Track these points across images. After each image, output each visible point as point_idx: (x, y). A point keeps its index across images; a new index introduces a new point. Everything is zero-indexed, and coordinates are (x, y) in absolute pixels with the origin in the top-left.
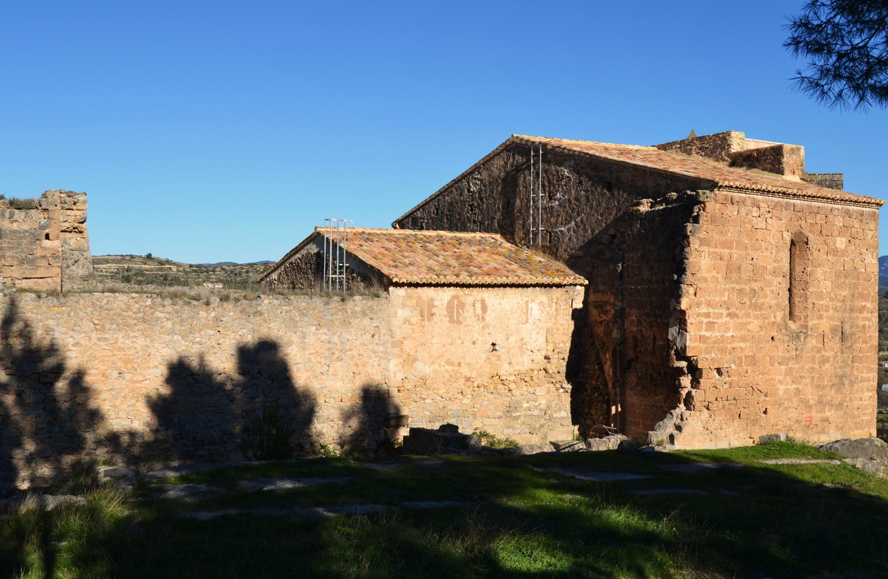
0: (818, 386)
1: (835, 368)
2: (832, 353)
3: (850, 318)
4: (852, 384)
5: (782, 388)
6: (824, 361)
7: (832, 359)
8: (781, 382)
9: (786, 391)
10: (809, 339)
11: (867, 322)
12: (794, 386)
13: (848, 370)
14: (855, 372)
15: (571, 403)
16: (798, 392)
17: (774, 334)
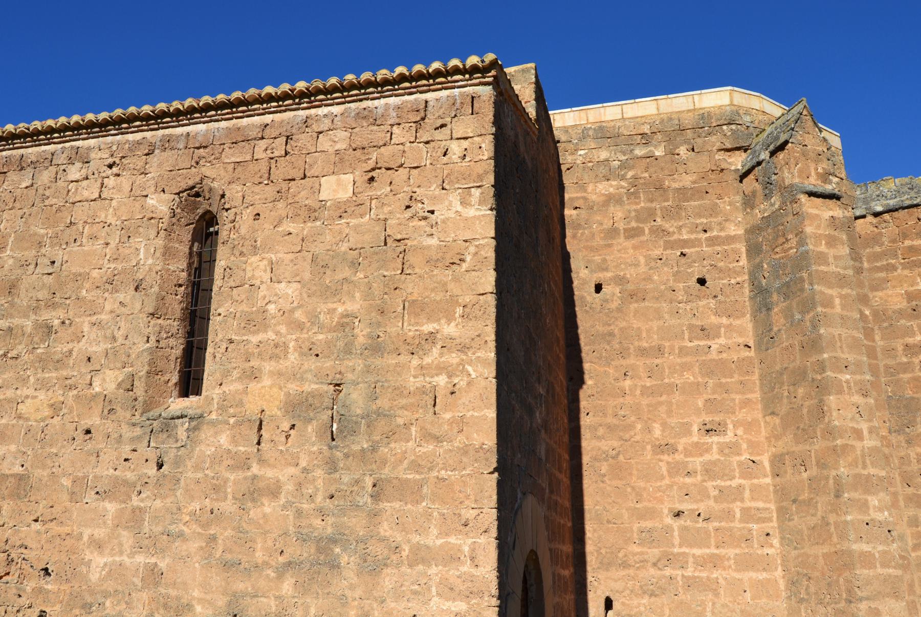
0: (227, 566)
1: (299, 513)
2: (292, 470)
3: (368, 370)
4: (372, 568)
5: (99, 562)
6: (254, 492)
7: (290, 487)
8: (98, 545)
9: (115, 572)
10: (206, 433)
11: (441, 380)
12: (140, 559)
13: (356, 523)
14: (385, 529)
15: (496, 347)
16: (154, 575)
17: (93, 420)
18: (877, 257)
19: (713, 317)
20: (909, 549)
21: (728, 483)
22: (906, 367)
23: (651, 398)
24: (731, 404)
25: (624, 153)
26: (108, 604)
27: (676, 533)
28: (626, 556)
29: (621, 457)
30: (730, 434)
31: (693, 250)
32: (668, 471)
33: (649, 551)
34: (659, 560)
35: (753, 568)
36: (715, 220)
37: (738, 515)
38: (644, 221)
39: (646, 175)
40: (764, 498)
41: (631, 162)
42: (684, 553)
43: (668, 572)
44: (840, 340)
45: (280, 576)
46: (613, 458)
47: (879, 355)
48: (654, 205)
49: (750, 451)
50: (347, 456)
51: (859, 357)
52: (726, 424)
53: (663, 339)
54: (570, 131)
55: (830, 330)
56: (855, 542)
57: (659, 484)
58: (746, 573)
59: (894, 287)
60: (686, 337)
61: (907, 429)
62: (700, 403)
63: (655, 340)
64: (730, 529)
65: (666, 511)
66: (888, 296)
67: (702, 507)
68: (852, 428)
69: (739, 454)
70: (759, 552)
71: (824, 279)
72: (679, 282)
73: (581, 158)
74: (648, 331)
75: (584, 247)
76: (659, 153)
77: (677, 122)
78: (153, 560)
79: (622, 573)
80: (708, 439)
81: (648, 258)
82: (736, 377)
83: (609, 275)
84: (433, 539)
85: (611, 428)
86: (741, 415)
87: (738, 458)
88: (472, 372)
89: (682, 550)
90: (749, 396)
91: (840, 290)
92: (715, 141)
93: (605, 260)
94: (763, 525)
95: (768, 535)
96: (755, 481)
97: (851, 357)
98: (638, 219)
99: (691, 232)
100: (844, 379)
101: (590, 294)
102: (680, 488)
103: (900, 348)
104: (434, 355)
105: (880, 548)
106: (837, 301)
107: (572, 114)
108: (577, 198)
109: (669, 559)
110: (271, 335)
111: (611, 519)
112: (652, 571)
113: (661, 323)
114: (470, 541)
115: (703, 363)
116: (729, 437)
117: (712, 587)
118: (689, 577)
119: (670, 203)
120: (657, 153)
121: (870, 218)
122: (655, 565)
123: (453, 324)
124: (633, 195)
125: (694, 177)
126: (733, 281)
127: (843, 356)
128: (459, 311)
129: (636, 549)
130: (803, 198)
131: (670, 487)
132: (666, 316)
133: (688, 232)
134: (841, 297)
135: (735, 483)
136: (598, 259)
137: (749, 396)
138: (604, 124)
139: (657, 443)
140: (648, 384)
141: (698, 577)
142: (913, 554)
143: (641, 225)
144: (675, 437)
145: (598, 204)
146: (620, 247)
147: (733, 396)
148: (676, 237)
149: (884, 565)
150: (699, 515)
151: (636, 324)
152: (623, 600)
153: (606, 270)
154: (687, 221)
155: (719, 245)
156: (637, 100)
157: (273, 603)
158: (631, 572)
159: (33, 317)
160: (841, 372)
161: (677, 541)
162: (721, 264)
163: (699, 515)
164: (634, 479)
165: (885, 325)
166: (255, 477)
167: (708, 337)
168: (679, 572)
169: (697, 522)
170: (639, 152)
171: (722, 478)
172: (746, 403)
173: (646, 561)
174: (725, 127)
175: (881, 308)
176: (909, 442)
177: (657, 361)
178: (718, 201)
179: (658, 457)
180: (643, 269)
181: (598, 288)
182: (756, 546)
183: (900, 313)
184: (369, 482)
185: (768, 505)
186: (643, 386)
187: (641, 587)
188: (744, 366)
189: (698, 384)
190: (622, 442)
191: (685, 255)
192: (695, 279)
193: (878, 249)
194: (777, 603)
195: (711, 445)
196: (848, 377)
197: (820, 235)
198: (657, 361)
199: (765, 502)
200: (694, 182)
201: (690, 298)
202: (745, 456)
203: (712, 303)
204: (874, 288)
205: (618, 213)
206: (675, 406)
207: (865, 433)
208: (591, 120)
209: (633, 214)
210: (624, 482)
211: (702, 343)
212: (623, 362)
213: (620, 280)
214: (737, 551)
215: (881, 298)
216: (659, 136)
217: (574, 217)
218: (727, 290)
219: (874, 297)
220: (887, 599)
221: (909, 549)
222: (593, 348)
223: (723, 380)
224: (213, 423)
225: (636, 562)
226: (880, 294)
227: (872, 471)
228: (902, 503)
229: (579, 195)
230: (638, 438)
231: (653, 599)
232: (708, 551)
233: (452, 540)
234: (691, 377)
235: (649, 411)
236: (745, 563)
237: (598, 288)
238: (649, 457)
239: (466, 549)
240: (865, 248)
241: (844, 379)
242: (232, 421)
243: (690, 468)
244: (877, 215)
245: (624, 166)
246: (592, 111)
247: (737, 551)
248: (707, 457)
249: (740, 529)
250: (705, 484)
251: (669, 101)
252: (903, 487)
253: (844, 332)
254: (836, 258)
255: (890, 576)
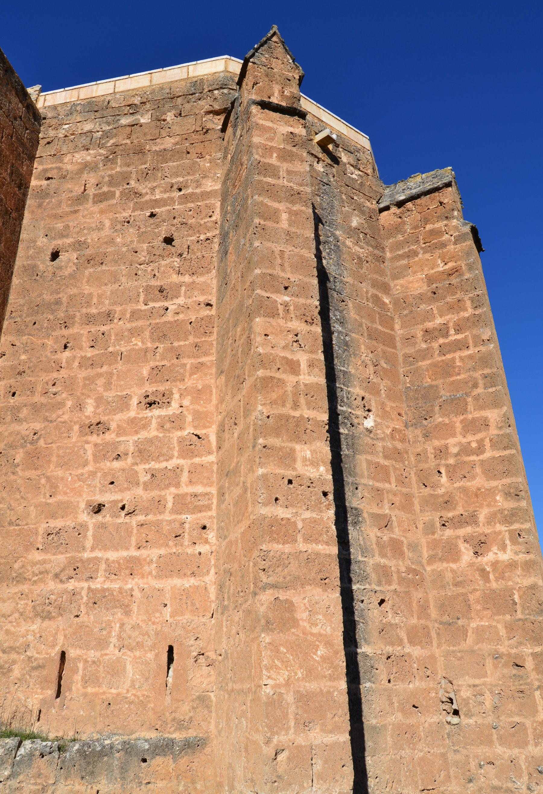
18: (399, 245)
19: (175, 276)
20: (424, 562)
21: (164, 465)
22: (425, 354)
23: (89, 370)
24: (182, 371)
25: (109, 124)
27: (90, 533)
28: (23, 566)
29: (41, 442)
30: (175, 405)
31: (164, 209)
32: (94, 456)
33: (53, 558)
34: (63, 570)
35: (180, 573)
36: (192, 178)
37: (170, 505)
38: (117, 185)
39: (128, 141)
40: (205, 481)
41: (114, 131)
42: (96, 558)
43: (71, 585)
44: (282, 257)
46: (31, 443)
47: (398, 344)
48: (129, 169)
49: (196, 423)
51: (307, 280)
52: (171, 393)
53: (115, 303)
54: (59, 108)
55: (269, 244)
56: (265, 505)
57: (80, 471)
58: (169, 581)
59: (415, 272)
60: (141, 299)
61: (424, 421)
62: (145, 372)
63: (106, 306)
64: (158, 523)
65: (83, 505)
66: (409, 283)
67: (126, 497)
68: (284, 358)
69: (181, 429)
70: (190, 551)
71: (269, 191)
72: (144, 242)
73: (64, 131)
74: (100, 296)
75: (48, 216)
76: (144, 120)
78: (263, 745)
79: (15, 589)
80: (148, 413)
81: (114, 222)
82: (191, 339)
83: (69, 241)
85: (36, 408)
86: (189, 383)
87: (179, 433)
89: (94, 555)
90: (203, 359)
91: (290, 206)
92: (205, 105)
93: (67, 227)
94: (199, 515)
95: (204, 528)
96: (197, 460)
97: (295, 278)
98: (110, 184)
99: (165, 191)
100: (279, 301)
101: (43, 262)
102: (105, 475)
103: (420, 334)
105: (307, 515)
106: (284, 216)
107: (64, 93)
108: (51, 169)
109: (76, 569)
111: (14, 519)
112: (52, 585)
113: (116, 286)
115: (156, 328)
116: (174, 409)
117: (121, 602)
118: (97, 589)
119: (147, 166)
120: (142, 121)
121: (394, 209)
125: (177, 139)
126: (202, 237)
127: (282, 274)
129: (38, 556)
130: (255, 109)
131: (93, 474)
132: (124, 280)
133: (161, 192)
134: (290, 212)
135: (170, 464)
136: (60, 226)
137: (203, 359)
138: (94, 99)
139: (87, 422)
140: (89, 355)
141: (108, 589)
142: (429, 569)
143: (112, 189)
144: (109, 414)
145: (72, 172)
146: (86, 212)
147: (185, 361)
148: (147, 198)
149: (307, 539)
150: (123, 508)
151: (87, 289)
152: (9, 627)
153: (67, 236)
154: (162, 182)
155: (193, 202)
156: (131, 76)
158: (25, 588)
160: (277, 291)
162: (192, 221)
163: (123, 508)
164: (52, 467)
165: (406, 312)
167: (166, 298)
168: (85, 585)
169: (118, 517)
170: (124, 121)
171: (157, 459)
172: (198, 368)
173: (47, 572)
174: (216, 92)
175: (401, 295)
176: (426, 436)
177: (103, 328)
178: (198, 160)
179: (85, 439)
180: (107, 232)
181: (55, 256)
182: (186, 543)
183: (421, 297)
185: (208, 489)
186: (82, 357)
187: (34, 607)
188: (202, 327)
189: (146, 351)
190: (47, 423)
191: (154, 215)
192: (161, 239)
193: (400, 237)
194: (204, 620)
195: (150, 421)
196: (287, 298)
197: (271, 147)
198: (103, 328)
199: (205, 485)
200: (177, 144)
201: (153, 258)
202: (189, 430)
203: (176, 262)
204: (396, 277)
205: (92, 179)
206: (115, 378)
207: (304, 366)
208: (82, 97)
209: (107, 179)
210: (39, 472)
211: (157, 305)
212: (65, 332)
213: (79, 245)
214: (162, 551)
215: (402, 286)
216: (148, 106)
217: (43, 188)
218: (193, 247)
219: (395, 285)
220: (308, 588)
221: (424, 562)
223: (176, 344)
225: (34, 574)
226: (401, 281)
227: (307, 413)
228: (417, 507)
229: (54, 166)
230: (66, 417)
231: (47, 623)
232: (125, 553)
234: (140, 344)
235: (85, 385)
236: (169, 567)
237: (55, 256)
238: (74, 440)
240: (388, 238)
241: (279, 301)
243: (121, 449)
244: (400, 204)
245: (107, 135)
246: (84, 89)
247: (162, 551)
248: (143, 435)
249: (170, 522)
250: (135, 468)
251: (163, 73)
252: (419, 488)
253: (288, 249)
254: (289, 172)
255: (318, 554)
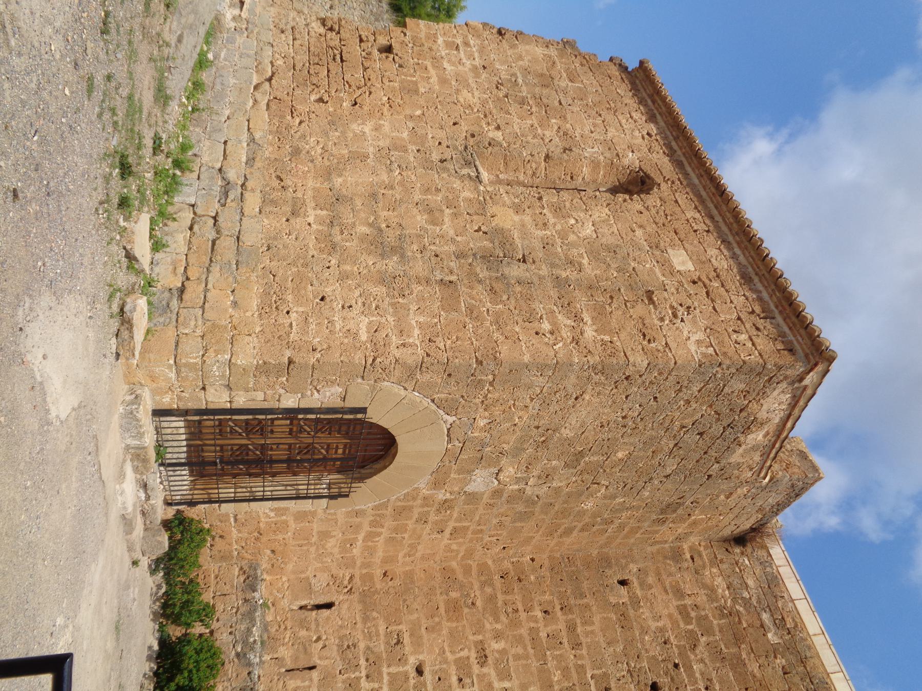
2: (452, 232)
3: (541, 278)
8: (377, 128)
25: (759, 602)
26: (337, 134)
32: (460, 658)
38: (699, 625)
41: (753, 609)
43: (362, 662)
45: (370, 225)
50: (470, 265)
53: (589, 647)
65: (421, 657)
74: (592, 632)
75: (658, 567)
77: (808, 655)
78: (371, 156)
81: (662, 630)
83: (639, 592)
84: (414, 319)
88: (558, 346)
89: (385, 676)
99: (702, 674)
104: (564, 321)
110: (552, 221)
111: (408, 602)
113: (604, 645)
114: (418, 342)
119: (725, 650)
120: (770, 635)
122: (368, 648)
123: (594, 334)
124: (722, 612)
128: (607, 338)
129: (382, 629)
131: (446, 661)
133: (700, 670)
138: (782, 585)
157: (350, 221)
159: (529, 96)
161: (393, 670)
166: (442, 211)
170: (765, 616)
173: (371, 639)
177: (565, 641)
180: (653, 625)
181: (623, 583)
184: (453, 278)
186: (538, 628)
201: (635, 675)
205: (702, 599)
208: (780, 569)
213: (635, 602)
222: (565, 579)
224: (476, 189)
230: (488, 626)
233: (417, 332)
237: (623, 583)
239: (411, 340)
242: (481, 198)
245: (747, 603)
251: (827, 646)
